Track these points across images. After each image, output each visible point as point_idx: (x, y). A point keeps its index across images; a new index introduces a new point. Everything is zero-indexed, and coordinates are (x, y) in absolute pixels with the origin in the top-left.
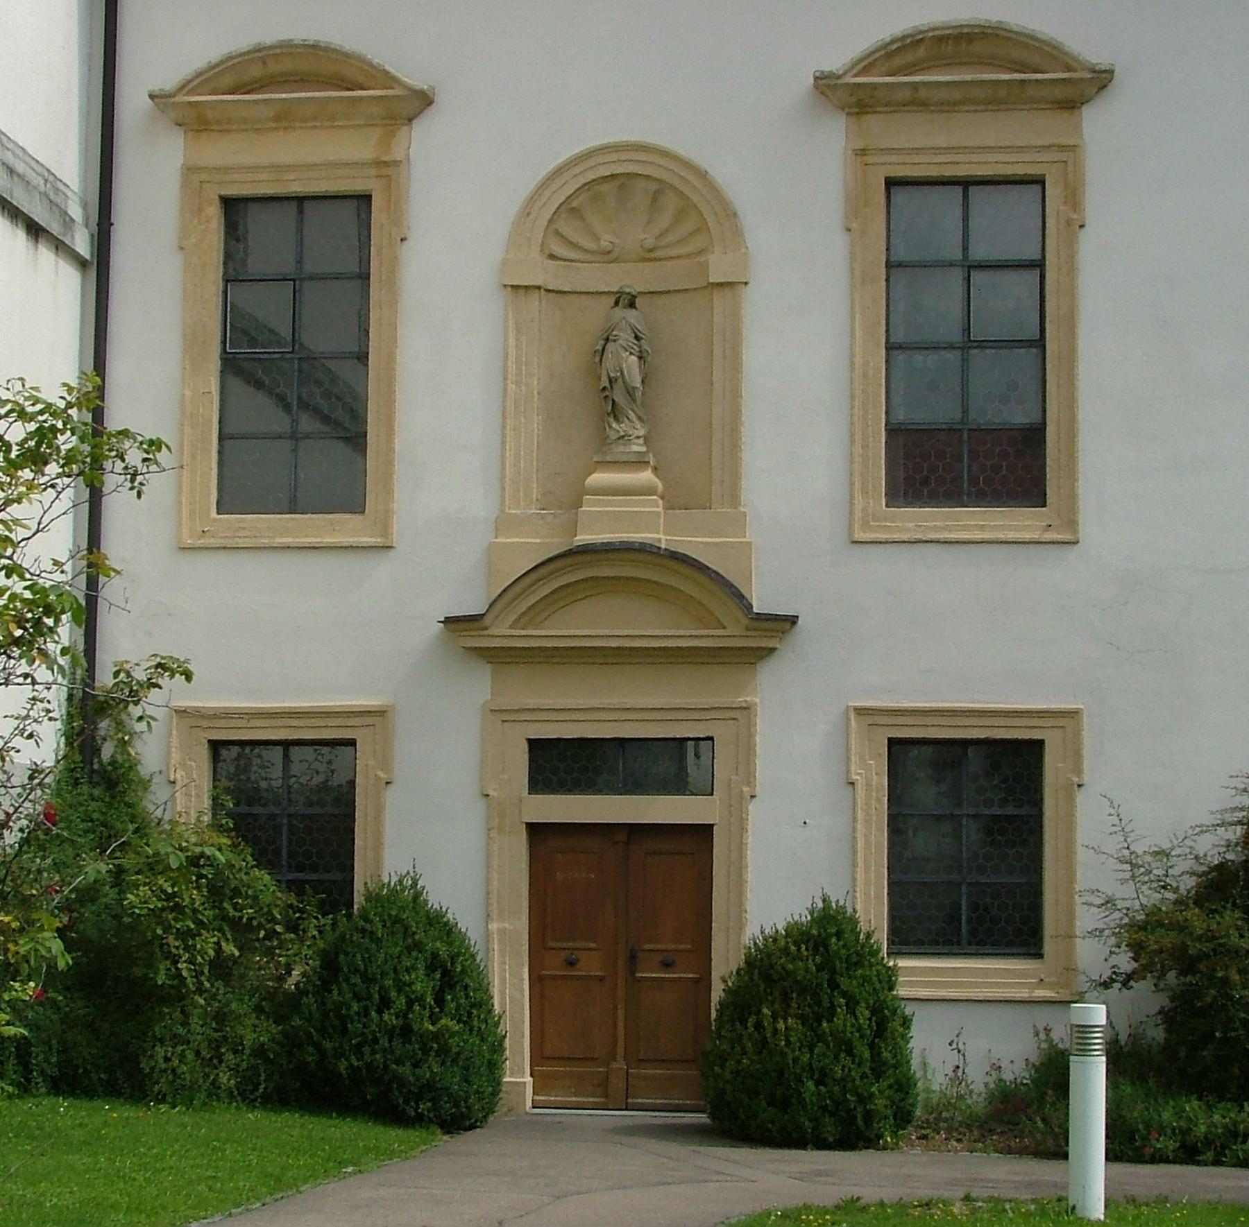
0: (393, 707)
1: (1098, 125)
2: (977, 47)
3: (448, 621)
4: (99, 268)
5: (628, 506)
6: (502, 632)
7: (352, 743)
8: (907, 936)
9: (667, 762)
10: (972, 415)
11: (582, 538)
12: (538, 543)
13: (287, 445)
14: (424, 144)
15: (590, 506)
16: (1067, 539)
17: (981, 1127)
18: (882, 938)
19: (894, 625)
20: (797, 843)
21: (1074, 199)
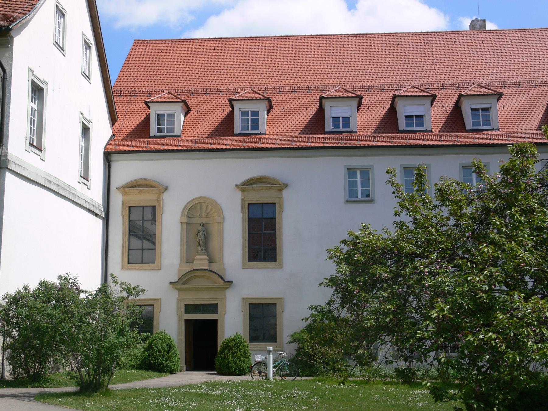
0: (161, 299)
1: (285, 193)
2: (264, 180)
3: (170, 283)
4: (106, 220)
5: (201, 262)
6: (180, 286)
7: (153, 305)
8: (253, 339)
9: (213, 308)
10: (150, 219)
11: (194, 268)
12: (187, 268)
13: (141, 251)
14: (166, 196)
15: (196, 262)
16: (280, 266)
17: (480, 175)
18: (247, 339)
19: (253, 282)
20: (232, 324)
21: (281, 207)
